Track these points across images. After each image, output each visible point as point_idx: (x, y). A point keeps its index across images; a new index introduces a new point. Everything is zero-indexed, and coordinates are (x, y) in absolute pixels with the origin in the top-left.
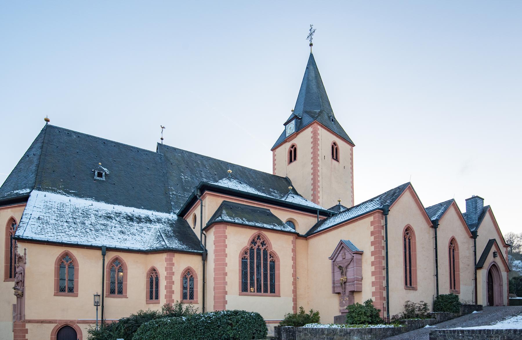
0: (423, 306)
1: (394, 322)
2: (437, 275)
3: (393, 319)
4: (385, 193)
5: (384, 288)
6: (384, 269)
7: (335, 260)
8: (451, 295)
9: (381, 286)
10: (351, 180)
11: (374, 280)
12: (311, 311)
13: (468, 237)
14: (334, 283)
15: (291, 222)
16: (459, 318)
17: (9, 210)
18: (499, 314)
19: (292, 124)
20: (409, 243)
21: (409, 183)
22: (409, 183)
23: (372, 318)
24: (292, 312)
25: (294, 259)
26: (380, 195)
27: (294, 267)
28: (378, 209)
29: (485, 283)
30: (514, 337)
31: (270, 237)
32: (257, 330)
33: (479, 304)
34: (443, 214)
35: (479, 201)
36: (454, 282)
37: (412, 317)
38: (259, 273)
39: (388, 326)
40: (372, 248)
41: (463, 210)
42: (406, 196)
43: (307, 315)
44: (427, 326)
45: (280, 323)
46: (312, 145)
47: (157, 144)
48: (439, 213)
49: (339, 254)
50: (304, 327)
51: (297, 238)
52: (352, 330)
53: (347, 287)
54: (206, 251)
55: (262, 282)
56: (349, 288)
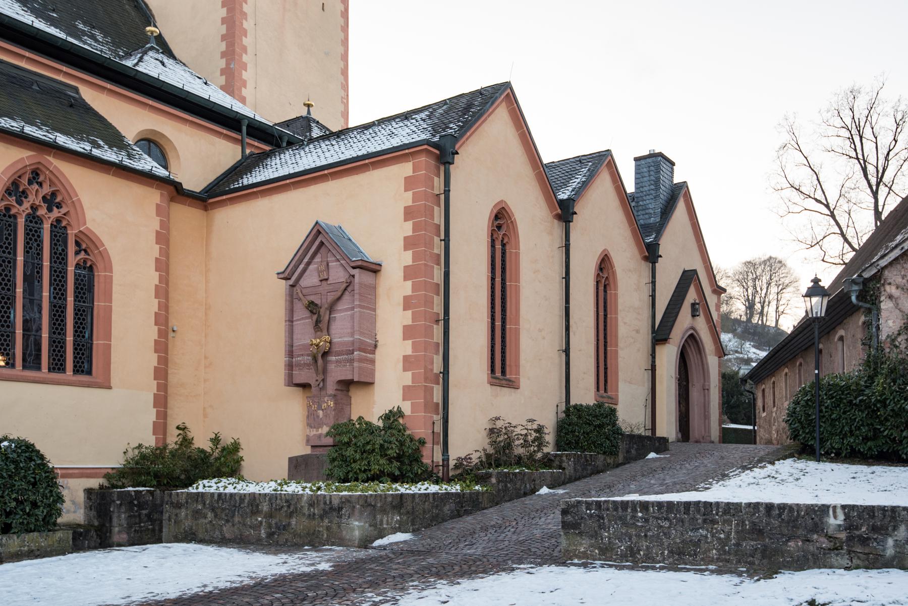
0: (534, 435)
1: (460, 478)
2: (567, 351)
3: (456, 467)
4: (444, 102)
5: (437, 376)
6: (437, 321)
8: (600, 406)
9: (428, 370)
10: (341, 50)
11: (409, 351)
12: (216, 440)
13: (638, 256)
14: (290, 353)
15: (152, 144)
16: (618, 471)
18: (708, 462)
21: (507, 85)
22: (507, 85)
23: (402, 463)
24: (150, 441)
25: (163, 266)
26: (429, 106)
27: (163, 292)
28: (427, 142)
29: (674, 379)
30: (768, 524)
31: (82, 183)
32: (19, 502)
33: (659, 433)
34: (585, 185)
35: (665, 167)
37: (508, 464)
39: (445, 488)
40: (407, 258)
41: (630, 187)
42: (497, 123)
43: (202, 451)
44: (544, 490)
45: (107, 476)
48: (575, 182)
49: (308, 264)
50: (191, 490)
51: (172, 199)
52: (347, 500)
53: (331, 367)
55: (45, 335)
56: (337, 372)
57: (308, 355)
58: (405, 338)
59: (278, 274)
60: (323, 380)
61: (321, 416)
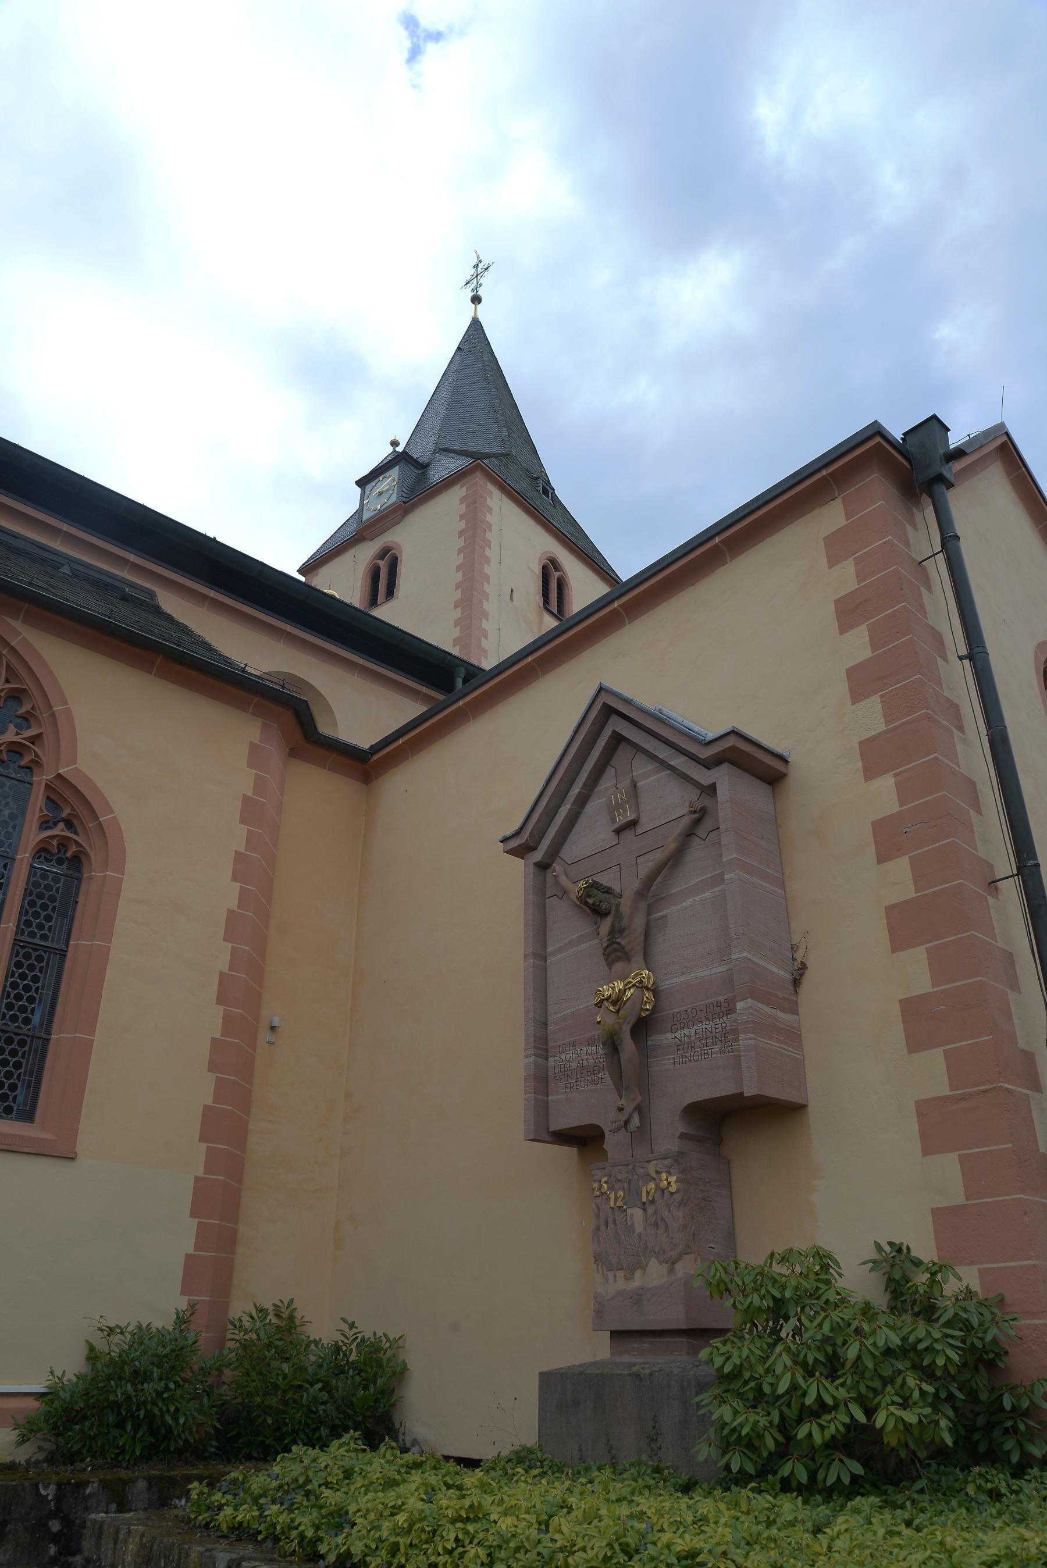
7: (555, 850)
11: (921, 983)
14: (541, 1044)
19: (389, 482)
46: (461, 543)
49: (583, 800)
57: (590, 1042)
59: (504, 840)
60: (639, 1109)
61: (639, 1228)
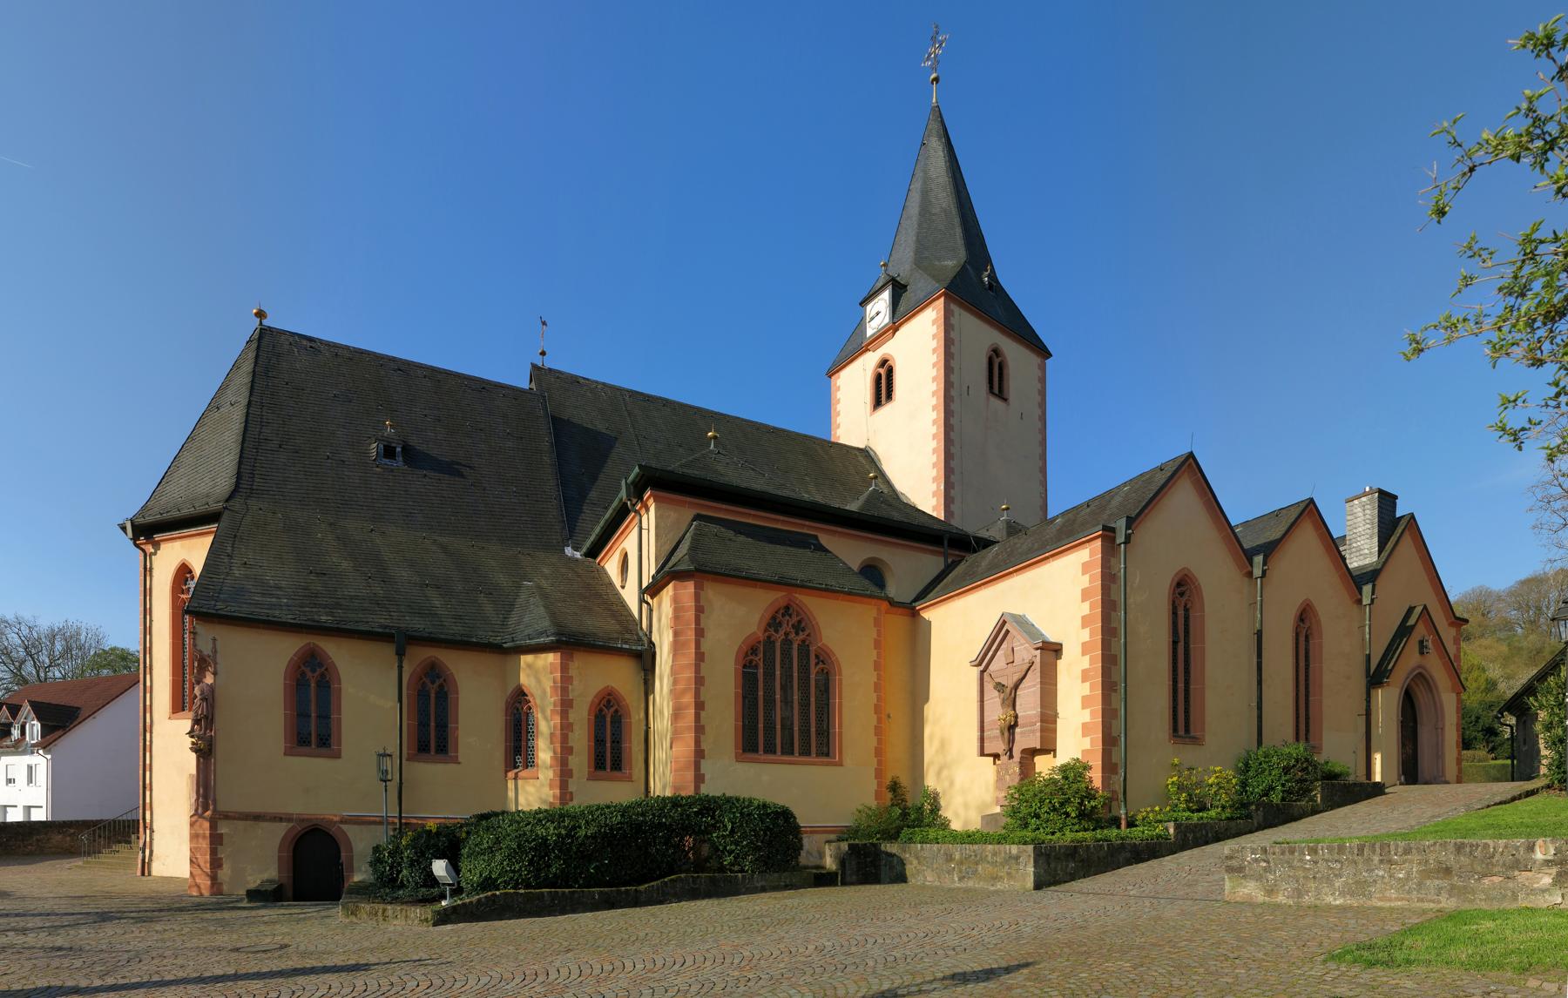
17: (177, 544)
20: (1187, 618)
36: (1305, 723)
38: (787, 702)
42: (1184, 494)
47: (529, 367)
53: (1017, 737)
54: (652, 644)
58: (1084, 707)
